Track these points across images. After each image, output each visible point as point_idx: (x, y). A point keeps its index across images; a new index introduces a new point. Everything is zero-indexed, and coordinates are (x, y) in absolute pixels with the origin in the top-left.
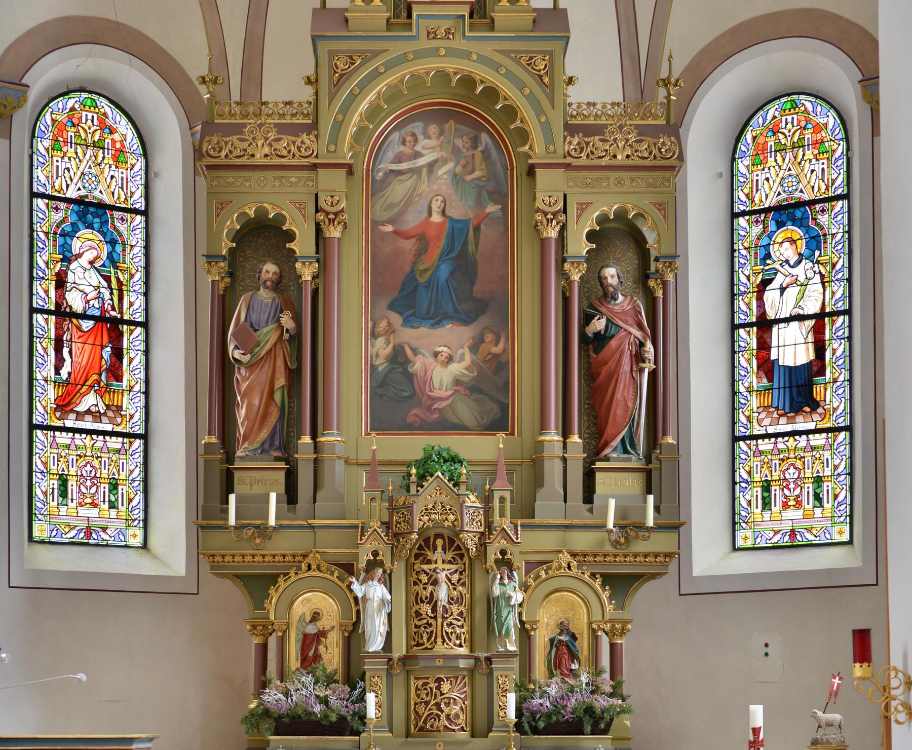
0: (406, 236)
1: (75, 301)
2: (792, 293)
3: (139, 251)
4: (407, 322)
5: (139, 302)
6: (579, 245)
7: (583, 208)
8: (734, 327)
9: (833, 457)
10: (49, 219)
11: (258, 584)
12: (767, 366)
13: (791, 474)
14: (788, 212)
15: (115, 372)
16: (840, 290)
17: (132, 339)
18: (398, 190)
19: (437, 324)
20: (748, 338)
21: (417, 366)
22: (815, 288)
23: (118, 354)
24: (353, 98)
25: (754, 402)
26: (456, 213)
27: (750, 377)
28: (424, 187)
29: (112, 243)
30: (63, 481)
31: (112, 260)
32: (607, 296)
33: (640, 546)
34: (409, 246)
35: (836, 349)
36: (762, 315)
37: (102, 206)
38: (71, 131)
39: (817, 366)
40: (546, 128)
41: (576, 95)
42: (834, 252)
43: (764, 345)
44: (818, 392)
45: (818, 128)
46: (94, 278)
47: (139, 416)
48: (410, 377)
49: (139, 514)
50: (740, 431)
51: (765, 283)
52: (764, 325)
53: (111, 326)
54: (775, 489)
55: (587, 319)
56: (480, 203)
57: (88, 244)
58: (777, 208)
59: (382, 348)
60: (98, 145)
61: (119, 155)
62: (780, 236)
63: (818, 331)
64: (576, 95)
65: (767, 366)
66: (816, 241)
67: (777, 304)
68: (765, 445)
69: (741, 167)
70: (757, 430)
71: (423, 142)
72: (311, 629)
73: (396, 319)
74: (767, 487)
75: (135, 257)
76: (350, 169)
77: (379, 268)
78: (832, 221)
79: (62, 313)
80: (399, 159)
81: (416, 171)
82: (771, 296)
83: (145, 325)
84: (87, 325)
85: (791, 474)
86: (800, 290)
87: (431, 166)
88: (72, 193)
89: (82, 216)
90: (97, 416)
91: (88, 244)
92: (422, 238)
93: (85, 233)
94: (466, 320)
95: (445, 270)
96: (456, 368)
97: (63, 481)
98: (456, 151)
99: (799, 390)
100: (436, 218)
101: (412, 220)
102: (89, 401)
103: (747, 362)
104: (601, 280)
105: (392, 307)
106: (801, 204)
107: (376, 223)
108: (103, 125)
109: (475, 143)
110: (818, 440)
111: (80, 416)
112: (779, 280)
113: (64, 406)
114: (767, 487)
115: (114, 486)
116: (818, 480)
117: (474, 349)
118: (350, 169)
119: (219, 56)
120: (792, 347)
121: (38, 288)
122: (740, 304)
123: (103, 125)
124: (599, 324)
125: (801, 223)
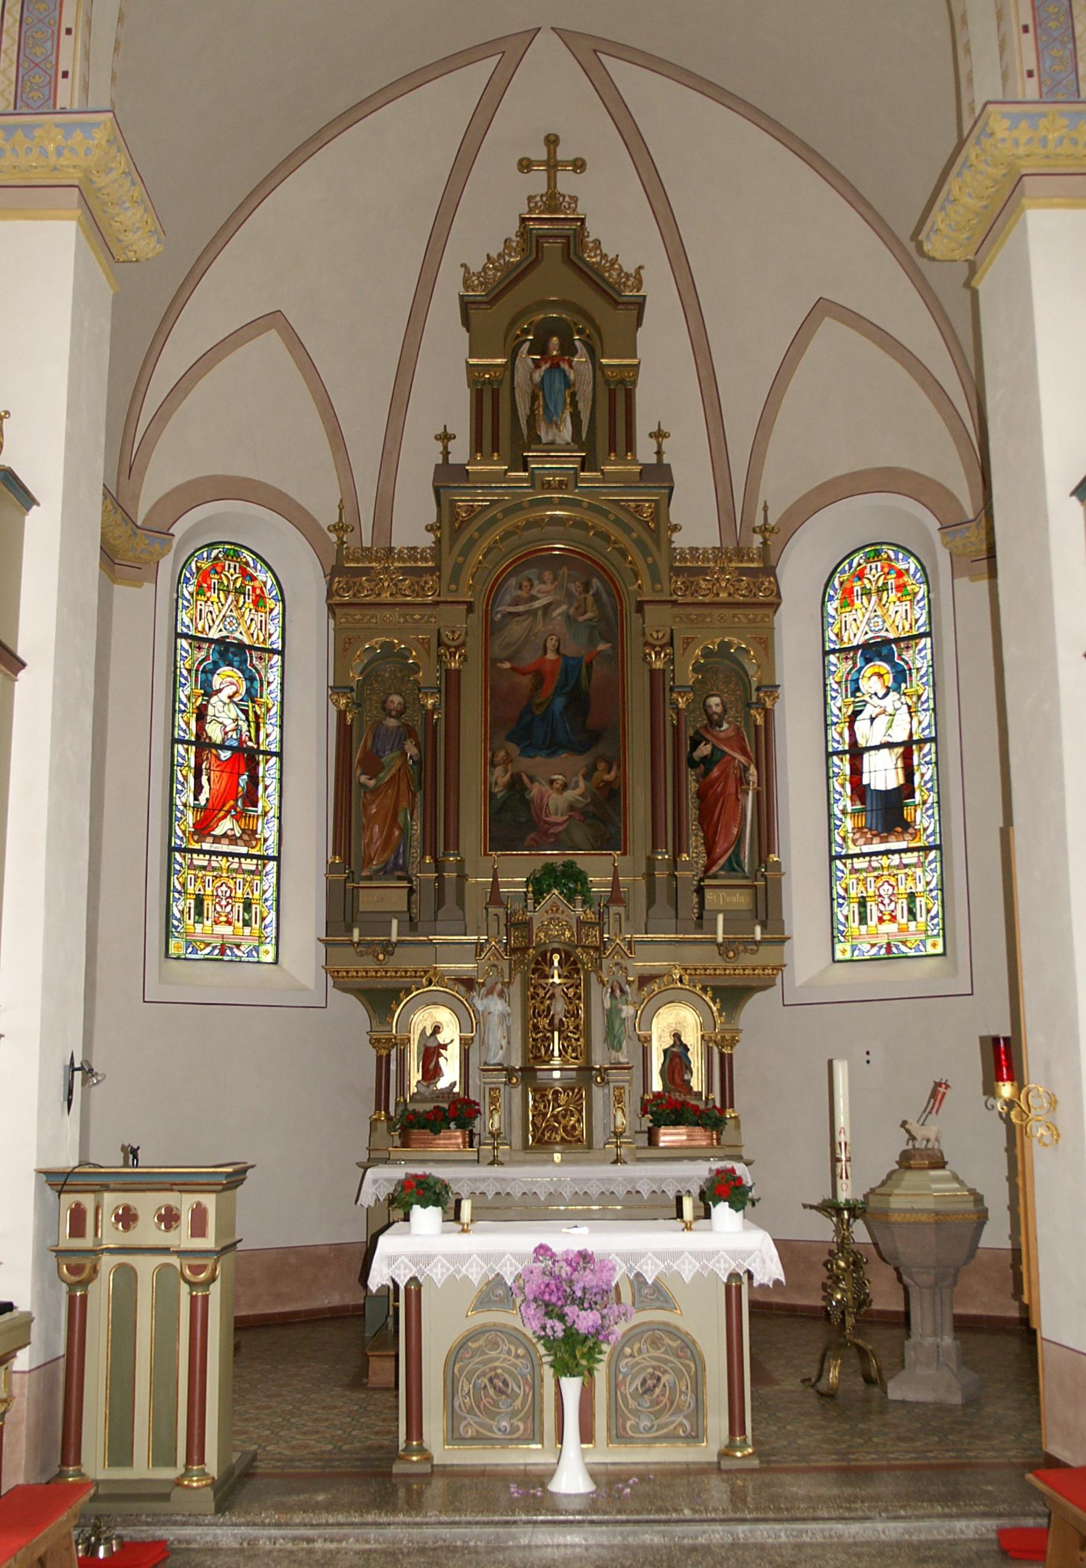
0: (523, 673)
1: (214, 732)
2: (882, 721)
3: (275, 686)
4: (524, 752)
5: (275, 733)
6: (688, 676)
7: (687, 642)
8: (829, 755)
9: (924, 878)
10: (189, 658)
11: (381, 1000)
12: (860, 791)
13: (886, 890)
14: (875, 650)
15: (251, 799)
16: (926, 718)
17: (268, 770)
18: (516, 630)
19: (552, 754)
20: (844, 766)
21: (535, 791)
22: (903, 715)
23: (254, 781)
24: (472, 543)
25: (849, 823)
26: (571, 649)
27: (845, 802)
28: (540, 627)
29: (251, 679)
30: (199, 900)
31: (251, 695)
32: (713, 722)
33: (747, 959)
34: (526, 681)
35: (924, 773)
36: (854, 742)
37: (241, 647)
38: (214, 579)
39: (907, 789)
40: (653, 569)
41: (680, 541)
42: (918, 684)
43: (857, 771)
44: (907, 813)
45: (900, 574)
46: (234, 711)
47: (273, 840)
48: (527, 803)
49: (271, 931)
50: (836, 849)
51: (856, 714)
52: (856, 753)
53: (247, 758)
54: (871, 905)
55: (695, 744)
56: (592, 643)
57: (227, 679)
58: (865, 646)
59: (501, 777)
60: (240, 591)
61: (259, 601)
62: (868, 671)
63: (907, 757)
64: (680, 541)
65: (860, 791)
66: (901, 675)
67: (866, 733)
68: (860, 864)
69: (831, 608)
70: (854, 850)
71: (538, 587)
72: (431, 1044)
73: (514, 749)
74: (862, 903)
75: (271, 694)
76: (470, 607)
77: (494, 694)
78: (919, 659)
79: (202, 744)
80: (516, 602)
81: (532, 613)
82: (861, 726)
83: (279, 755)
84: (225, 755)
85: (886, 890)
86: (887, 719)
87: (546, 608)
88: (214, 634)
89: (222, 655)
90: (233, 840)
91: (227, 679)
92: (539, 676)
93: (225, 670)
94: (580, 749)
95: (559, 703)
96: (570, 794)
97: (199, 900)
98: (569, 595)
99: (888, 812)
100: (551, 656)
101: (528, 659)
102: (226, 825)
103: (842, 787)
104: (706, 708)
105: (509, 738)
106: (887, 642)
107: (495, 661)
108: (244, 574)
109: (587, 586)
110: (910, 858)
111: (217, 839)
112: (868, 712)
113: (203, 828)
114: (862, 903)
115: (248, 906)
116: (912, 896)
117: (587, 777)
118: (470, 607)
119: (348, 503)
120: (882, 773)
121: (180, 720)
122: (833, 733)
123: (244, 574)
124: (704, 750)
125: (888, 659)
